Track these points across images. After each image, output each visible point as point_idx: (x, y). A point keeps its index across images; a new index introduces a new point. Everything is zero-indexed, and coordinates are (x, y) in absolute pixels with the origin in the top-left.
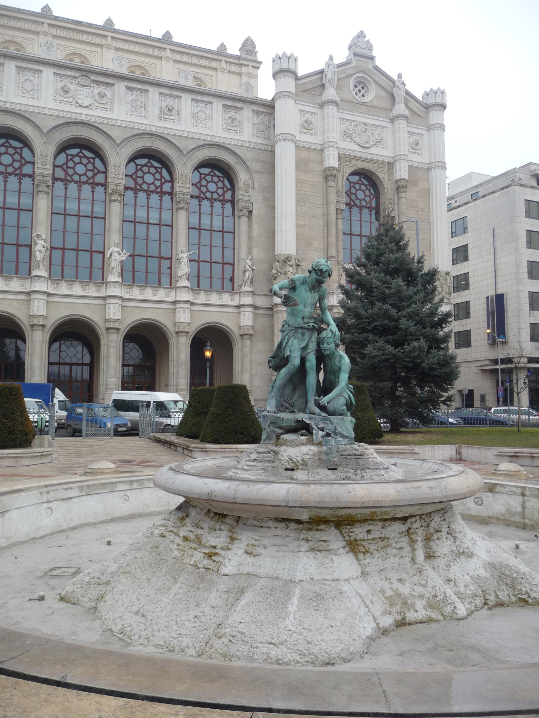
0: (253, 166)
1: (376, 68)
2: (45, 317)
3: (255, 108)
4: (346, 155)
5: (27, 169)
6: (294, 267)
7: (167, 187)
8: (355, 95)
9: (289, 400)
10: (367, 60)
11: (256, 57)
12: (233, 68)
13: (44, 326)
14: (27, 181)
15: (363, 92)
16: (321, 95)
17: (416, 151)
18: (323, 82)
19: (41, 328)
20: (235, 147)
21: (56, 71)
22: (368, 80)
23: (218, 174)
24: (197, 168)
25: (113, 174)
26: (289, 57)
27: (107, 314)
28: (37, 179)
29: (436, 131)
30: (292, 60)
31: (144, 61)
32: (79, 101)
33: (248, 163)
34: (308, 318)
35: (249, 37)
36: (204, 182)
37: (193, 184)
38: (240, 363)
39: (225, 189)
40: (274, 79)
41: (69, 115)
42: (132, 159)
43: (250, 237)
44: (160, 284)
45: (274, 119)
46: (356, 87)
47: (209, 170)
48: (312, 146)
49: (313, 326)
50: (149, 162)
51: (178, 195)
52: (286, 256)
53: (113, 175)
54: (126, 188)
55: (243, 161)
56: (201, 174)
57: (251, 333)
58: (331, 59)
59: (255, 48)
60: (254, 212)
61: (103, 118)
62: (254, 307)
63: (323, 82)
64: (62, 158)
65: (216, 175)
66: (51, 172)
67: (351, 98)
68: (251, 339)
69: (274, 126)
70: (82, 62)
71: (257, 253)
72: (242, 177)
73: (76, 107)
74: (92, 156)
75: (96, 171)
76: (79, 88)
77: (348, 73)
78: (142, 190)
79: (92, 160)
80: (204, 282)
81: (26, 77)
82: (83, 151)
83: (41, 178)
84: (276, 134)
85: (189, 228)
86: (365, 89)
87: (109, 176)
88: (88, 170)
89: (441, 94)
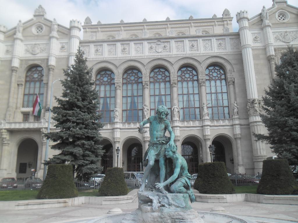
0: (232, 62)
1: (289, 6)
2: (120, 138)
3: (230, 37)
4: (278, 48)
5: (140, 80)
6: (258, 104)
7: (167, 79)
8: (279, 20)
9: (153, 184)
10: (283, 4)
11: (230, 16)
12: (220, 23)
13: (119, 142)
14: (140, 85)
15: (283, 18)
16: (261, 24)
17: (64, 51)
18: (262, 18)
19: (239, 139)
20: (223, 55)
21: (121, 43)
22: (285, 12)
23: (217, 68)
24: (207, 68)
25: (172, 77)
26: (243, 12)
27: (204, 133)
28: (172, 82)
29: (75, 39)
30: (245, 13)
31: (158, 31)
32: (157, 51)
33: (230, 61)
34: (159, 138)
35: (226, 9)
36: (211, 73)
37: (206, 75)
38: (236, 152)
39: (221, 74)
40: (238, 22)
41: (154, 57)
42: (180, 69)
43: (235, 93)
44: (195, 119)
45: (240, 40)
46: (279, 16)
47: (158, 70)
48: (258, 48)
49: (162, 142)
50: (214, 68)
51: (200, 80)
52: (253, 100)
53: (201, 76)
54: (178, 81)
55: (228, 61)
56: (209, 70)
57: (240, 137)
58: (264, 7)
59: (229, 12)
60: (236, 82)
61: (110, 58)
62: (241, 125)
63: (262, 18)
64: (125, 76)
65: (216, 69)
66: (177, 79)
67: (277, 22)
68: (240, 140)
69: (240, 43)
70: (206, 33)
71: (239, 100)
72: (228, 67)
73: (156, 53)
74: (164, 71)
75: (193, 75)
76: (157, 46)
77: (274, 11)
78: (184, 81)
79: (191, 71)
80: (216, 117)
81: (138, 46)
82: (215, 67)
83: (230, 79)
84: (242, 46)
85: (150, 96)
86: (284, 17)
87: (171, 77)
88: (217, 76)
89: (77, 23)
